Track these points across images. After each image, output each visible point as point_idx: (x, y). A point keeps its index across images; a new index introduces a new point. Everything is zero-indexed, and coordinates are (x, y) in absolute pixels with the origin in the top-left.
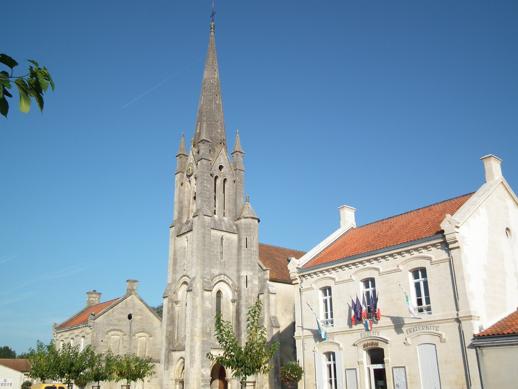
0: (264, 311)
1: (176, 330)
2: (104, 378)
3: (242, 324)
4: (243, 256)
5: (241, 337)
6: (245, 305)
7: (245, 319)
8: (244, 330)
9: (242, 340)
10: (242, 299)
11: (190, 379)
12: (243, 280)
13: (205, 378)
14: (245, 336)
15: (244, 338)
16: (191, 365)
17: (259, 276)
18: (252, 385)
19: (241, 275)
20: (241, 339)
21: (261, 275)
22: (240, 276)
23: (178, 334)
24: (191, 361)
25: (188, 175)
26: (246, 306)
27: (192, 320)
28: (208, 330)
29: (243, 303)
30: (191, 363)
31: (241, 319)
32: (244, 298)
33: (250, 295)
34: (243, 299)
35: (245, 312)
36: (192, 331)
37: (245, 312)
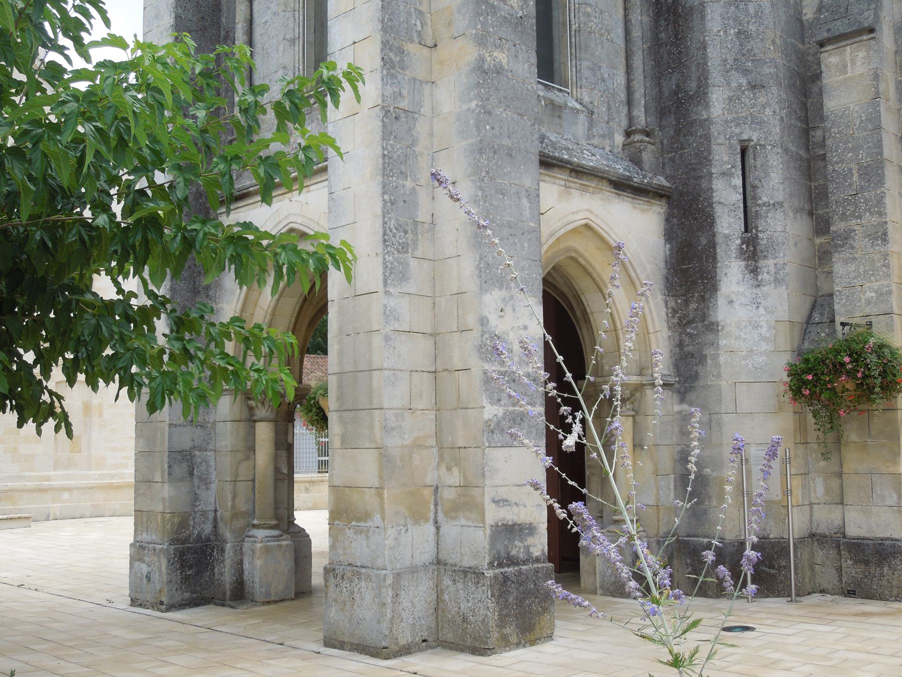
5: (707, 106)
9: (714, 129)
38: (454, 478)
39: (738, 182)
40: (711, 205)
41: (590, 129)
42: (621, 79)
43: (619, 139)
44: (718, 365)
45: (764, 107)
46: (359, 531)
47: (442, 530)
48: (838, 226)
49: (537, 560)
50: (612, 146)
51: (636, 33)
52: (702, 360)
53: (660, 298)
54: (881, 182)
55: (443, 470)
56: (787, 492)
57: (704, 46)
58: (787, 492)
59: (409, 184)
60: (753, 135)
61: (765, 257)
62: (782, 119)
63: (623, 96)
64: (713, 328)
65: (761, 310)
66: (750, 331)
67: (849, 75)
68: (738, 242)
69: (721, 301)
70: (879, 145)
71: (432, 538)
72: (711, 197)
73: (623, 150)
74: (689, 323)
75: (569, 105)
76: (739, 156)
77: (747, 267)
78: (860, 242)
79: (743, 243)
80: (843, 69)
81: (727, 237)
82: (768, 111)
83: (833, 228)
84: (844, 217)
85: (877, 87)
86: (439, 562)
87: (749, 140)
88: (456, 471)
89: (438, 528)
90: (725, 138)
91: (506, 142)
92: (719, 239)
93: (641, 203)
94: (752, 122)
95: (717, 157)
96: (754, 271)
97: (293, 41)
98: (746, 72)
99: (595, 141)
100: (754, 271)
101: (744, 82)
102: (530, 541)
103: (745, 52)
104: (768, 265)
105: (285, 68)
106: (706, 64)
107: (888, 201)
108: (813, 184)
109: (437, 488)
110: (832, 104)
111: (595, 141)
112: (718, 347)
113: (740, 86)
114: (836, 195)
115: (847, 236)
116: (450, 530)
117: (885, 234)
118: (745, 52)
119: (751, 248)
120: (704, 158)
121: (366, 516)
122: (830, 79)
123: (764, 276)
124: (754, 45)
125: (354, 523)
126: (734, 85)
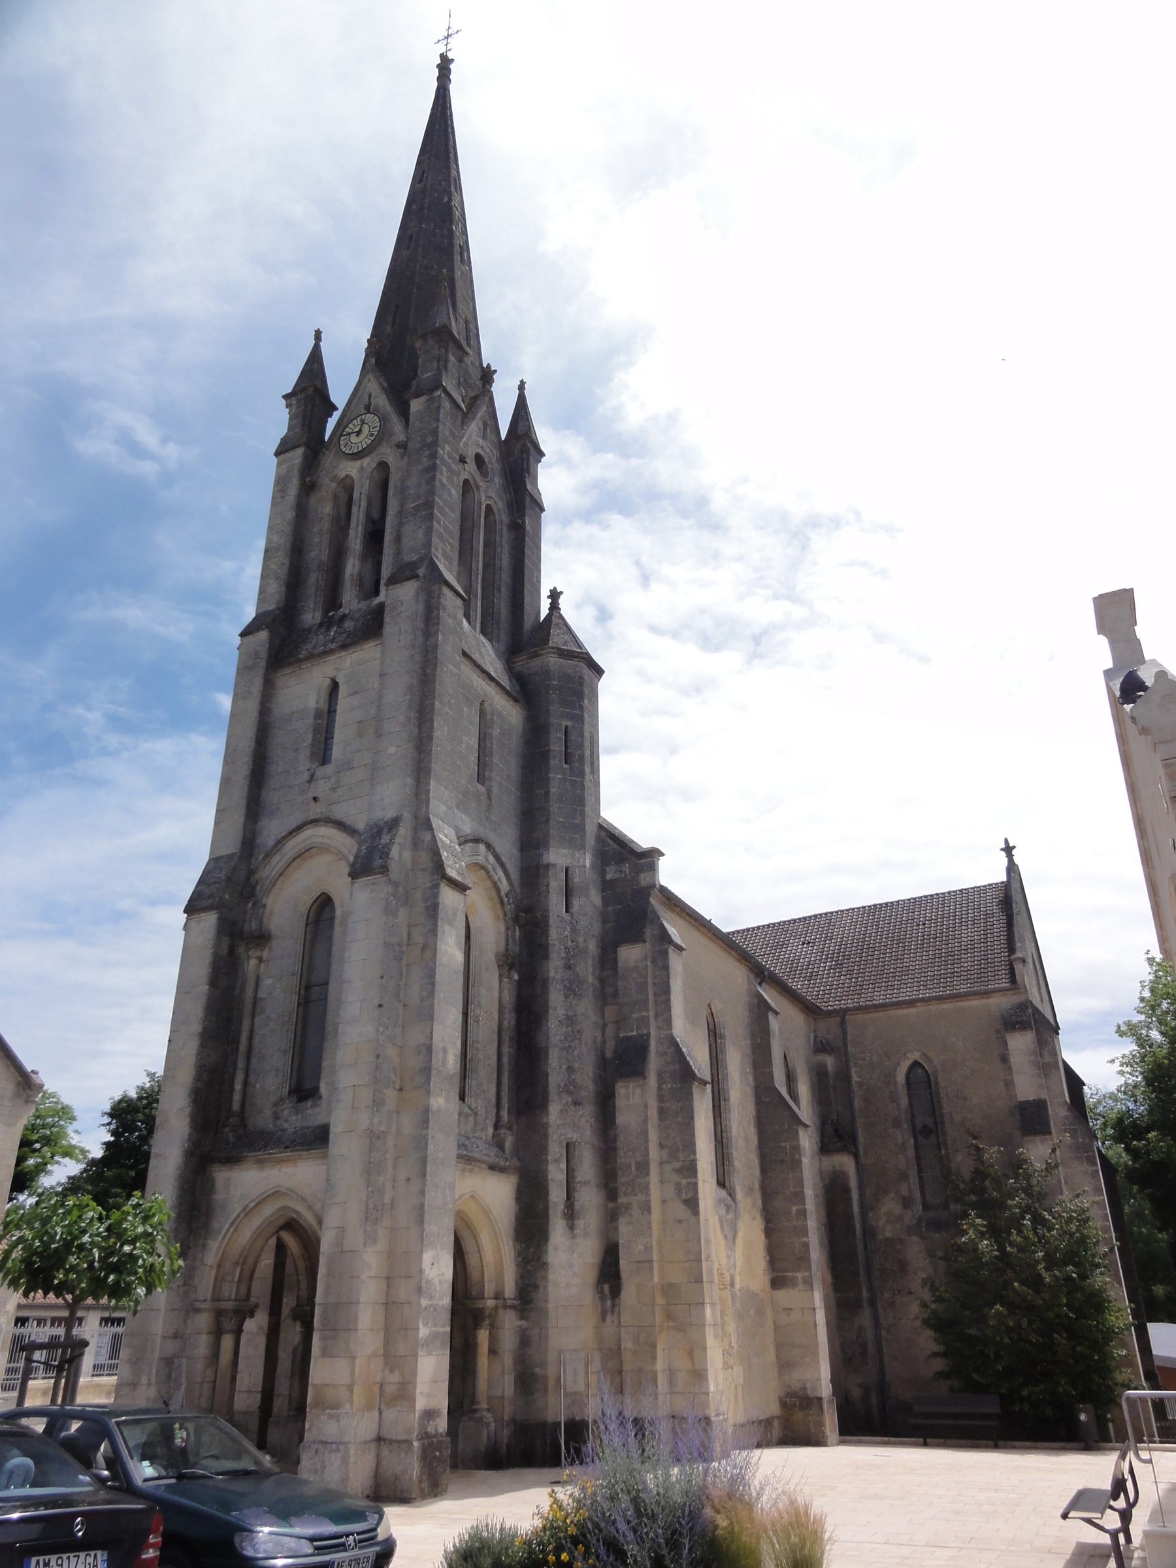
0: (644, 1013)
1: (241, 1064)
2: (386, 1363)
3: (550, 1061)
4: (553, 790)
5: (547, 1114)
6: (562, 981)
7: (563, 1038)
8: (559, 1086)
9: (550, 1130)
10: (551, 956)
11: (362, 1306)
12: (556, 884)
13: (434, 1301)
14: (561, 1111)
15: (560, 1122)
16: (368, 1229)
17: (609, 877)
18: (223, 1303)
19: (545, 861)
20: (546, 1126)
21: (617, 875)
22: (538, 867)
23: (246, 1084)
24: (367, 1207)
25: (344, 450)
26: (565, 987)
27: (380, 1006)
28: (451, 1062)
29: (556, 972)
30: (366, 1218)
31: (548, 1038)
32: (559, 953)
33: (582, 945)
34: (553, 955)
35: (563, 1012)
36: (378, 1056)
37: (563, 1012)
38: (395, 1378)
39: (563, 1166)
40: (547, 1180)
41: (475, 1126)
42: (493, 1090)
43: (491, 1130)
44: (547, 1294)
45: (581, 1117)
46: (331, 1417)
47: (384, 1414)
48: (622, 1200)
49: (441, 1435)
50: (487, 1136)
51: (505, 1060)
52: (536, 1287)
53: (511, 1243)
54: (648, 1174)
55: (387, 1371)
56: (587, 1386)
57: (547, 1075)
58: (587, 1386)
59: (381, 1179)
60: (573, 1136)
61: (578, 1218)
62: (591, 1125)
63: (494, 1101)
64: (544, 1266)
65: (575, 1255)
66: (654, 1456)
67: (631, 1102)
68: (562, 1207)
69: (551, 1249)
70: (647, 1150)
71: (377, 1420)
72: (547, 1176)
73: (493, 1138)
74: (529, 1262)
75: (465, 1111)
76: (565, 1149)
77: (567, 1224)
78: (635, 1212)
79: (565, 1208)
80: (627, 1097)
81: (556, 1203)
82: (583, 1120)
83: (619, 1200)
84: (626, 1194)
85: (646, 1113)
86: (379, 1439)
87: (572, 1138)
88: (397, 1372)
89: (380, 1413)
90: (634, 1470)
91: (441, 1155)
92: (551, 1205)
93: (503, 1176)
94: (574, 1126)
95: (551, 1149)
96: (571, 1227)
97: (285, 1052)
98: (570, 1093)
99: (477, 1134)
100: (571, 1227)
101: (570, 1100)
102: (438, 1420)
103: (571, 1080)
104: (580, 1223)
105: (277, 1070)
106: (547, 1087)
107: (652, 1187)
108: (608, 1166)
109: (382, 1385)
110: (620, 1119)
111: (477, 1134)
112: (547, 1281)
113: (567, 1103)
114: (622, 1179)
115: (628, 1207)
116: (390, 1414)
117: (650, 1208)
118: (571, 1080)
119: (570, 1212)
120: (544, 1148)
121: (337, 1406)
122: (620, 1102)
123: (577, 1231)
124: (577, 1077)
125: (327, 1411)
126: (564, 1101)
